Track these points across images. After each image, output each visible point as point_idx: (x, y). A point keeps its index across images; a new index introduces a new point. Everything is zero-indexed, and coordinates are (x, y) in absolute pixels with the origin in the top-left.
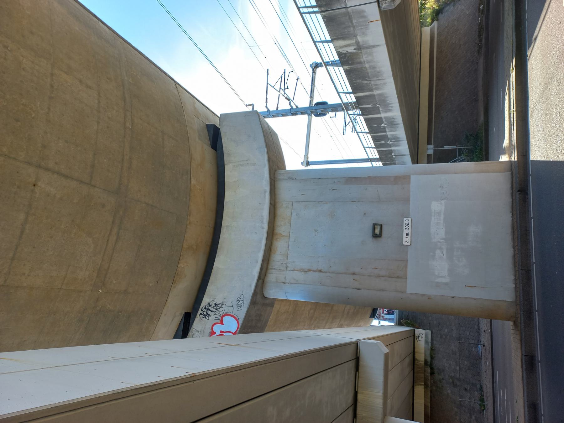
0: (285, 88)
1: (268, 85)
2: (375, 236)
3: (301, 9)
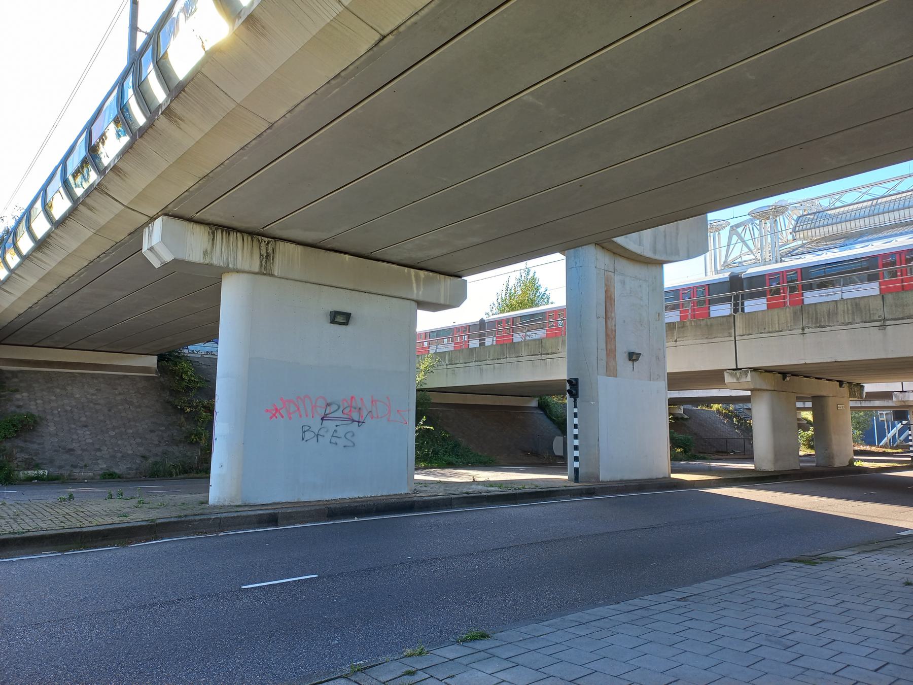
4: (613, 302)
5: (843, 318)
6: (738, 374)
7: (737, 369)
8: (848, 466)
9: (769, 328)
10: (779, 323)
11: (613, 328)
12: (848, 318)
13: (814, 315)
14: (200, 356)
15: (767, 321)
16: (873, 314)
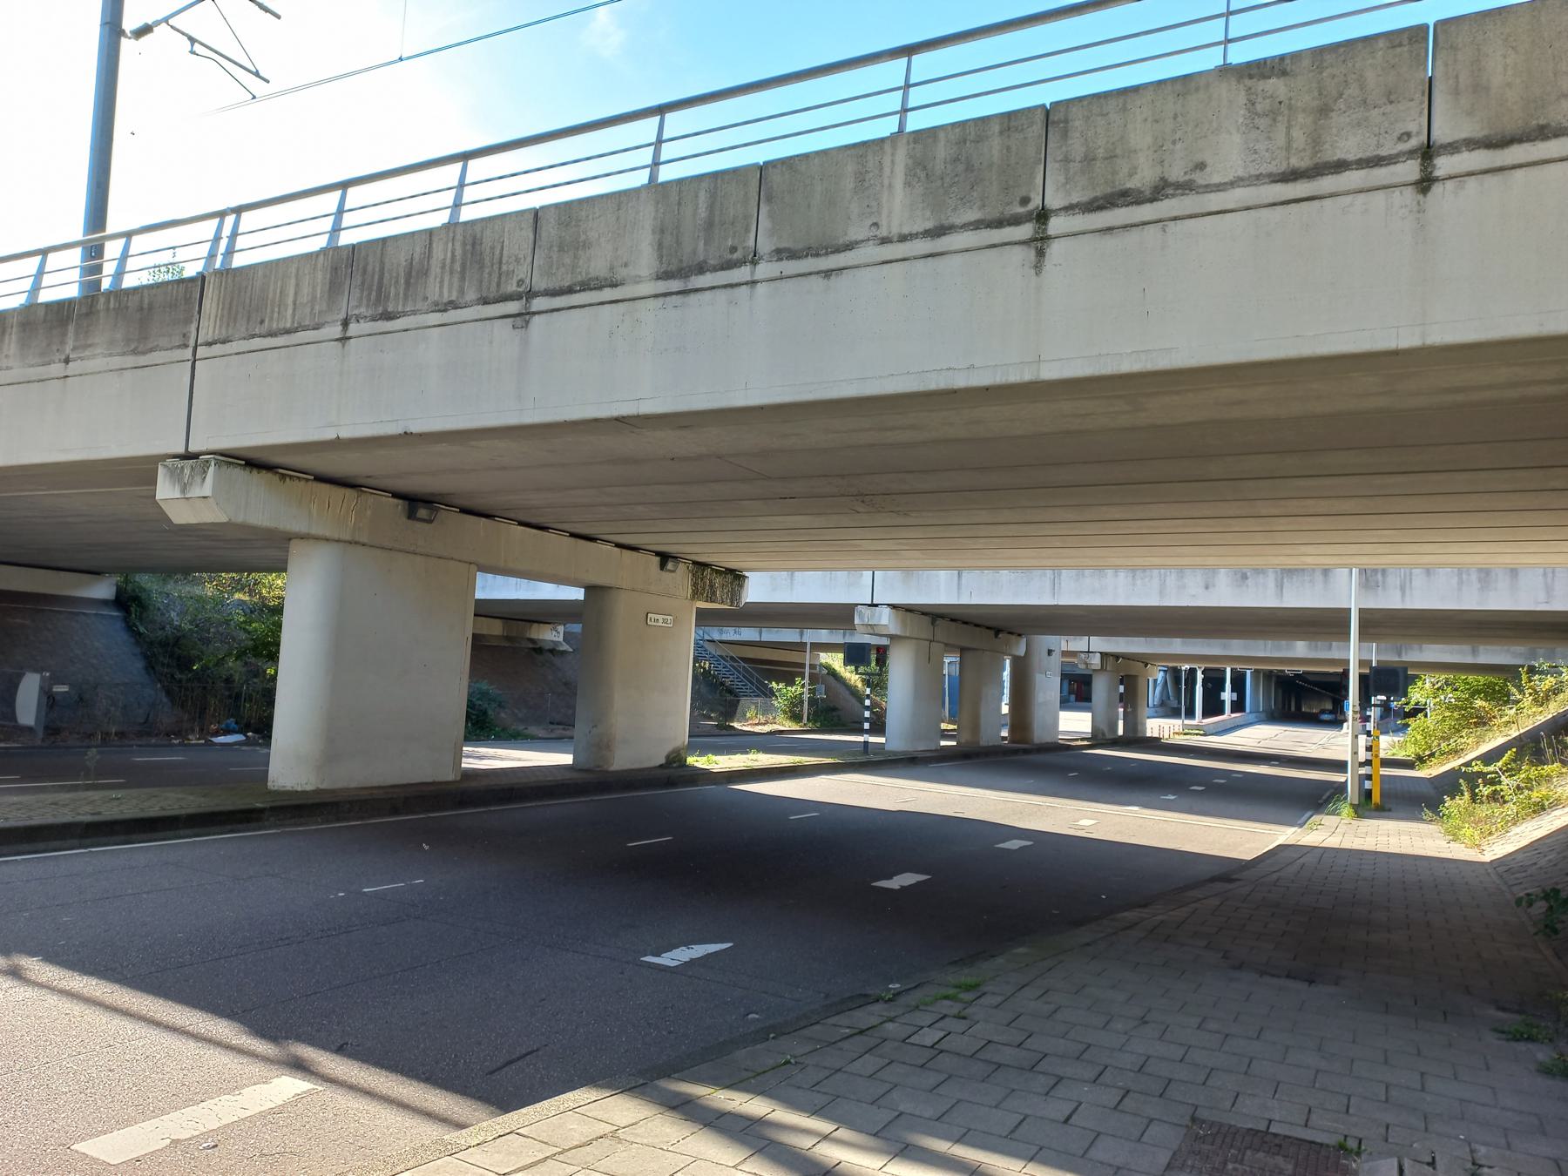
5: (438, 285)
6: (187, 471)
8: (661, 766)
9: (271, 319)
10: (295, 304)
12: (450, 291)
13: (376, 277)
15: (270, 296)
16: (508, 273)
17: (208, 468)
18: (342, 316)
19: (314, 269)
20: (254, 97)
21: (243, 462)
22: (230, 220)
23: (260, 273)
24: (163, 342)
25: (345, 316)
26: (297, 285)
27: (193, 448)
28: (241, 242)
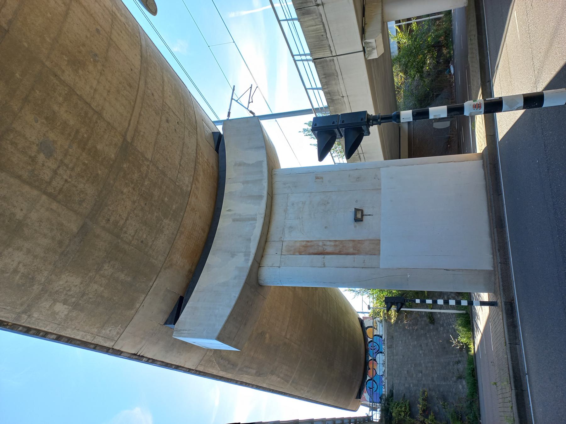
0: (250, 101)
1: (233, 100)
2: (325, 227)
3: (295, 57)
4: (309, 244)
6: (368, 49)
7: (364, 50)
9: (321, 32)
10: (315, 25)
11: (333, 244)
14: (386, 380)
15: (314, 35)
17: (367, 42)
18: (316, 7)
19: (305, 22)
20: (257, 87)
21: (363, 35)
22: (297, 58)
23: (309, 40)
24: (333, 68)
25: (316, 6)
26: (310, 26)
27: (362, 49)
28: (302, 53)
